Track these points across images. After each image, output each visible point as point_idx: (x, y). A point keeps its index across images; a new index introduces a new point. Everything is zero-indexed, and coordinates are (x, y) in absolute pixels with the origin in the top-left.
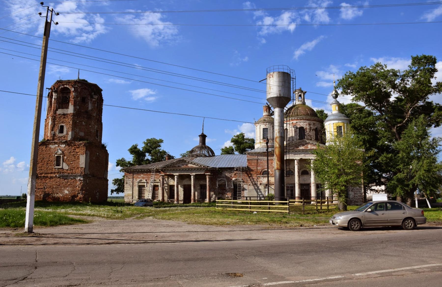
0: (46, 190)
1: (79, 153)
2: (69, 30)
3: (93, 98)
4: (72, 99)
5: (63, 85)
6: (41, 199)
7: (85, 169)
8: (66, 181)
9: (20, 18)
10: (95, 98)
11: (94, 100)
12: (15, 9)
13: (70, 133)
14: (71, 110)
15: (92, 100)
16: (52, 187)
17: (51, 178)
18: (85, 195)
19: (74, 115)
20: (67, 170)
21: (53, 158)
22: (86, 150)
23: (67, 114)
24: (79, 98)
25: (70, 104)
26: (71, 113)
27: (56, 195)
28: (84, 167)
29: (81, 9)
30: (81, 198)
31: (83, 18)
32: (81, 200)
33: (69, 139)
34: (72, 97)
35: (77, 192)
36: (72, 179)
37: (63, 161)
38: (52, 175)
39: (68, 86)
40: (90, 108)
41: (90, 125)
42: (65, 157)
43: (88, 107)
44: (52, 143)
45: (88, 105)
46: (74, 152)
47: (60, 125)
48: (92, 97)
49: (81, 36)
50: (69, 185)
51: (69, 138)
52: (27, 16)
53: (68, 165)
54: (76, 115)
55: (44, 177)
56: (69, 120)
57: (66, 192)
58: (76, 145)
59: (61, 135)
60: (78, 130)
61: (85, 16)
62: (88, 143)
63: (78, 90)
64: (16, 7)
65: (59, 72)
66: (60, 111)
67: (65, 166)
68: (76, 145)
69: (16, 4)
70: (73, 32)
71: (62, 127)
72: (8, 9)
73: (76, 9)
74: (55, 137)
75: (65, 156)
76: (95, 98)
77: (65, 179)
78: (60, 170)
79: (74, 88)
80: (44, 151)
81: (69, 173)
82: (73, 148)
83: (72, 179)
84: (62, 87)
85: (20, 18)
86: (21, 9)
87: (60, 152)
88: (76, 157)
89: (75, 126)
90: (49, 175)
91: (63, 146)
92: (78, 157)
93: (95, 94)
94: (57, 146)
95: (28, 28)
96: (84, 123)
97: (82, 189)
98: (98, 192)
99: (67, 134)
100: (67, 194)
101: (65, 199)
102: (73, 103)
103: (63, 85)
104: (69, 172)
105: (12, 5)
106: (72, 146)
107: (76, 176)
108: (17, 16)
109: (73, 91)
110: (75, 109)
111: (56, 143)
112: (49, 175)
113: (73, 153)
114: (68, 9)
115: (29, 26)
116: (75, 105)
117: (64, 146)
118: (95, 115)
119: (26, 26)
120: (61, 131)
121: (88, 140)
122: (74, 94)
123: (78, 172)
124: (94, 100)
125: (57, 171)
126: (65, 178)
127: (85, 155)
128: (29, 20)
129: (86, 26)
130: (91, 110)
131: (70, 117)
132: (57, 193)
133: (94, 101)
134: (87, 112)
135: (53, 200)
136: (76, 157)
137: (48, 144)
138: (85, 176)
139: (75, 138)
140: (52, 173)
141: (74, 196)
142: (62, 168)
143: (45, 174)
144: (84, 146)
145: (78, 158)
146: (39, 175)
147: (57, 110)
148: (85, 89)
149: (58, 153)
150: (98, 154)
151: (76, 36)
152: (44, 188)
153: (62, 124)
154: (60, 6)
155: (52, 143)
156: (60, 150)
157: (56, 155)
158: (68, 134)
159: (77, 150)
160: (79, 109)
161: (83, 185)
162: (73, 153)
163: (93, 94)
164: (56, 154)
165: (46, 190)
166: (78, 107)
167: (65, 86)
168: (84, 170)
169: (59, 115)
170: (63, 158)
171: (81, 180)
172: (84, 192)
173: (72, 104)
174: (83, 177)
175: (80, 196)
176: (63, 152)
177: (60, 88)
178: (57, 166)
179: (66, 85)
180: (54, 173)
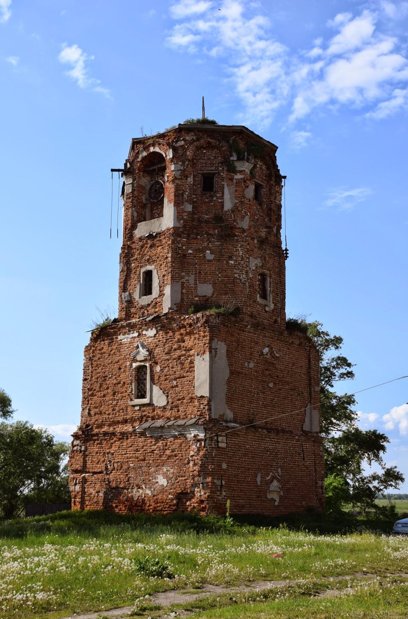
0: (111, 477)
1: (192, 352)
2: (361, 91)
3: (236, 172)
4: (170, 188)
5: (146, 148)
6: (100, 507)
7: (210, 400)
8: (160, 444)
9: (255, 94)
10: (241, 172)
11: (239, 176)
12: (242, 77)
13: (168, 290)
14: (168, 219)
15: (231, 179)
16: (125, 467)
17: (124, 436)
18: (214, 490)
19: (176, 232)
20: (164, 408)
21: (128, 376)
22: (211, 340)
23: (159, 234)
24: (190, 180)
25: (166, 200)
26: (169, 229)
27: (136, 494)
28: (207, 394)
29: (384, 32)
30: (202, 502)
31: (392, 52)
32: (203, 509)
33: (165, 311)
34: (171, 178)
35: (190, 482)
36: (175, 437)
37: (152, 379)
38: (129, 428)
39: (157, 149)
40: (228, 206)
41: (230, 258)
42: (158, 369)
43: (222, 205)
44: (123, 327)
45: (222, 197)
46: (179, 348)
47: (143, 270)
48: (232, 170)
49: (390, 98)
50: (169, 457)
51: (166, 306)
52: (269, 83)
53: (166, 392)
54: (185, 230)
55: (105, 434)
56: (164, 251)
57: (162, 481)
58: (184, 326)
59: (146, 300)
60: (192, 279)
61: (396, 45)
62: (219, 315)
63: (184, 154)
64: (244, 70)
65: (350, 196)
66: (142, 230)
67: (158, 398)
68: (184, 326)
69: (243, 65)
70: (373, 93)
71: (148, 275)
72: (229, 79)
73: (374, 35)
74: (133, 310)
75: (157, 363)
76: (241, 172)
77: (157, 439)
78: (147, 411)
79: (175, 150)
80: (106, 355)
81: (168, 419)
82: (177, 336)
83: (175, 437)
84: (145, 154)
85: (255, 94)
86: (254, 74)
87: (143, 353)
88: (187, 365)
89: (181, 264)
90: (120, 429)
91: (151, 332)
92: (192, 362)
93: (239, 159)
94: (136, 334)
95: (273, 110)
96: (209, 255)
97: (203, 471)
98: (273, 478)
99: (161, 295)
100: (163, 490)
101: (160, 506)
102: (172, 197)
103: (146, 148)
104: (168, 414)
105: (236, 70)
106: (174, 332)
107: (184, 427)
108: (247, 91)
109: (172, 160)
110: (179, 216)
111: (132, 327)
112: (120, 429)
113: (178, 353)
114: (355, 42)
115: (276, 105)
116: (177, 204)
117: (154, 332)
118: (245, 224)
119: (269, 106)
120: (147, 290)
121: (218, 307)
122: (173, 167)
123: (192, 411)
124: (239, 176)
125: (138, 414)
126: (158, 434)
127: (207, 356)
128: (273, 92)
129: (399, 71)
130: (233, 211)
131: (167, 242)
132: (139, 487)
133: (239, 181)
134: (219, 219)
135: (130, 509)
136: (187, 365)
137: (116, 334)
138: (212, 425)
139: (180, 307)
140: (125, 421)
141: (183, 496)
142: (150, 404)
143: (110, 425)
144: (203, 325)
145: (191, 369)
146: (96, 431)
147: (134, 227)
148: (210, 146)
149: (139, 358)
150: (266, 350)
151: (378, 101)
152: (107, 469)
153: (149, 268)
154: (337, 39)
155: (123, 327)
156: (143, 346)
157: (135, 365)
158: (164, 296)
159: (189, 342)
160: (193, 213)
161: (205, 456)
162: (178, 353)
163: (234, 158)
164: (134, 360)
165: (111, 477)
166: (189, 208)
167: (152, 149)
168: (209, 404)
169: (140, 239)
170: (152, 371)
171: (199, 440)
172: (209, 479)
173: (170, 201)
174: (206, 430)
175: (200, 493)
176: (150, 352)
177: (139, 159)
178: (138, 397)
179: (153, 145)
180: (133, 420)
